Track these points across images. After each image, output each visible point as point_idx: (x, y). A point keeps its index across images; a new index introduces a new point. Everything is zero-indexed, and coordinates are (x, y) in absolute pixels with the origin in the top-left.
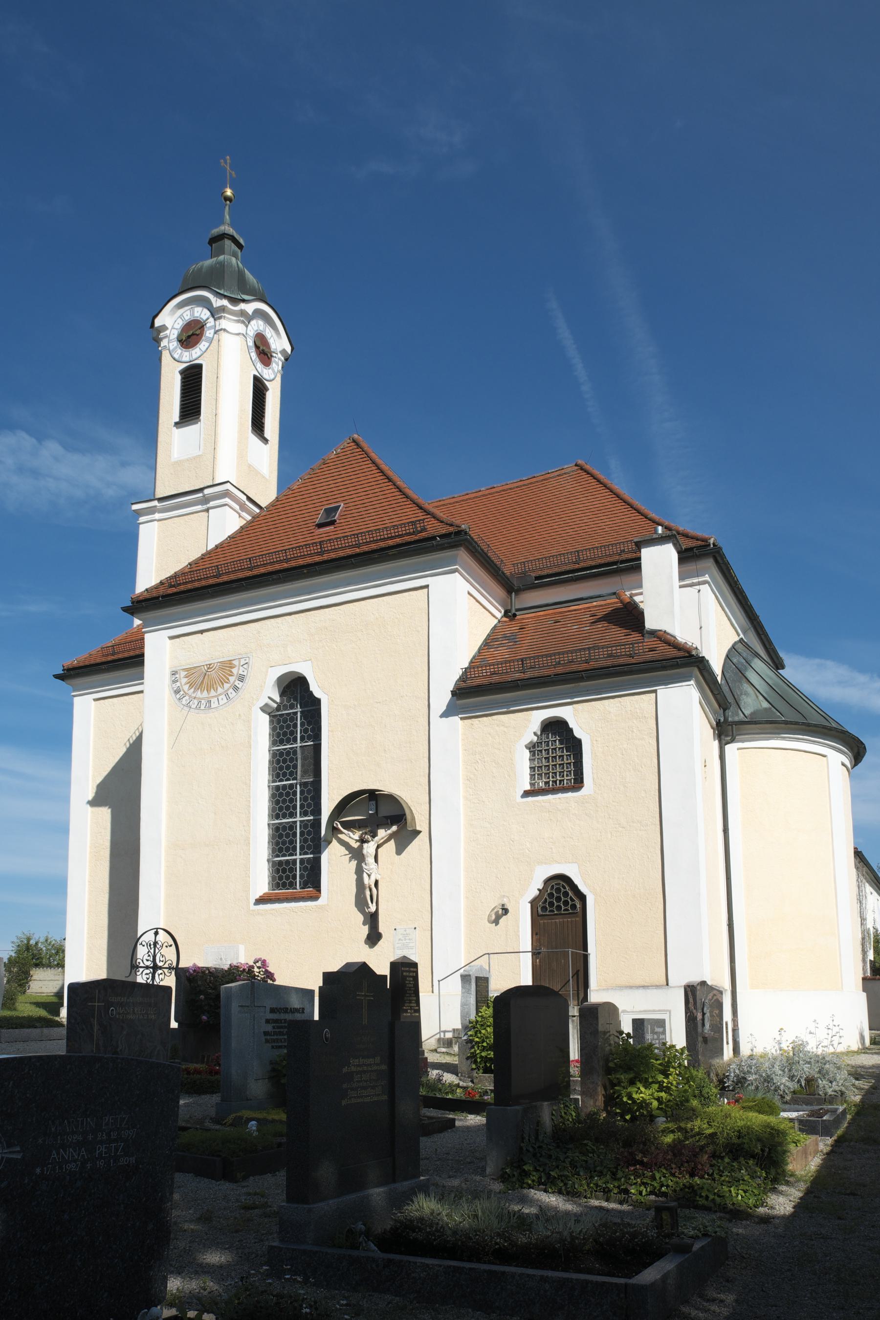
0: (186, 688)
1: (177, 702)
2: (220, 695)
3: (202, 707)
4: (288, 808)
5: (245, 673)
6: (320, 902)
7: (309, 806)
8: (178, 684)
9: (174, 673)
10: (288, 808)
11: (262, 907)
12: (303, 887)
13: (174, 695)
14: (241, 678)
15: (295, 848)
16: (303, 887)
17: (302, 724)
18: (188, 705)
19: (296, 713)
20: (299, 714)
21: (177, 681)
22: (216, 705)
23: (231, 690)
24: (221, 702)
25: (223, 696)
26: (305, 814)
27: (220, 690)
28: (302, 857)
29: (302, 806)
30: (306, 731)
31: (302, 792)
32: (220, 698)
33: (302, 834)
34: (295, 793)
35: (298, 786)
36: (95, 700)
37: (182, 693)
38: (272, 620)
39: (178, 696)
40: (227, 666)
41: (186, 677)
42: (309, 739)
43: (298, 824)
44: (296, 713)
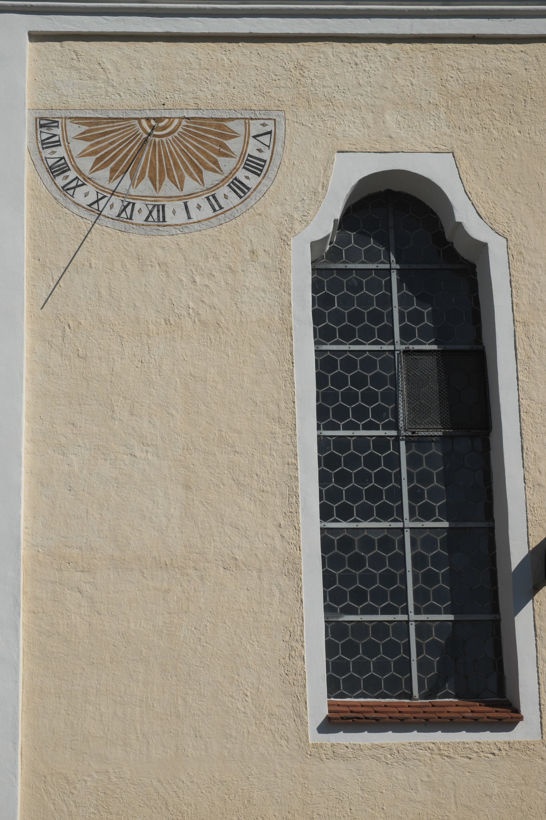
0: (86, 164)
1: (58, 195)
2: (191, 195)
3: (139, 218)
4: (374, 495)
5: (266, 155)
6: (520, 733)
7: (434, 494)
8: (60, 152)
9: (44, 123)
10: (374, 495)
11: (342, 738)
12: (430, 693)
13: (46, 176)
14: (257, 166)
15: (402, 596)
16: (430, 693)
17: (403, 301)
18: (95, 209)
19: (388, 271)
20: (394, 276)
21: (57, 144)
22: (181, 217)
23: (225, 189)
24: (195, 215)
25: (202, 201)
26: (426, 513)
27: (190, 185)
28: (423, 617)
29: (414, 494)
30: (416, 317)
31: (412, 461)
32: (192, 204)
33: (418, 561)
34: (394, 461)
35: (403, 444)
36: (36, 37)
37: (72, 174)
38: (339, 46)
39: (60, 181)
40: (209, 135)
41: (82, 137)
42: (425, 336)
43: (407, 535)
44: (388, 271)
